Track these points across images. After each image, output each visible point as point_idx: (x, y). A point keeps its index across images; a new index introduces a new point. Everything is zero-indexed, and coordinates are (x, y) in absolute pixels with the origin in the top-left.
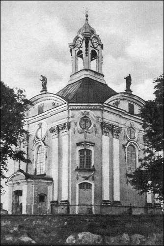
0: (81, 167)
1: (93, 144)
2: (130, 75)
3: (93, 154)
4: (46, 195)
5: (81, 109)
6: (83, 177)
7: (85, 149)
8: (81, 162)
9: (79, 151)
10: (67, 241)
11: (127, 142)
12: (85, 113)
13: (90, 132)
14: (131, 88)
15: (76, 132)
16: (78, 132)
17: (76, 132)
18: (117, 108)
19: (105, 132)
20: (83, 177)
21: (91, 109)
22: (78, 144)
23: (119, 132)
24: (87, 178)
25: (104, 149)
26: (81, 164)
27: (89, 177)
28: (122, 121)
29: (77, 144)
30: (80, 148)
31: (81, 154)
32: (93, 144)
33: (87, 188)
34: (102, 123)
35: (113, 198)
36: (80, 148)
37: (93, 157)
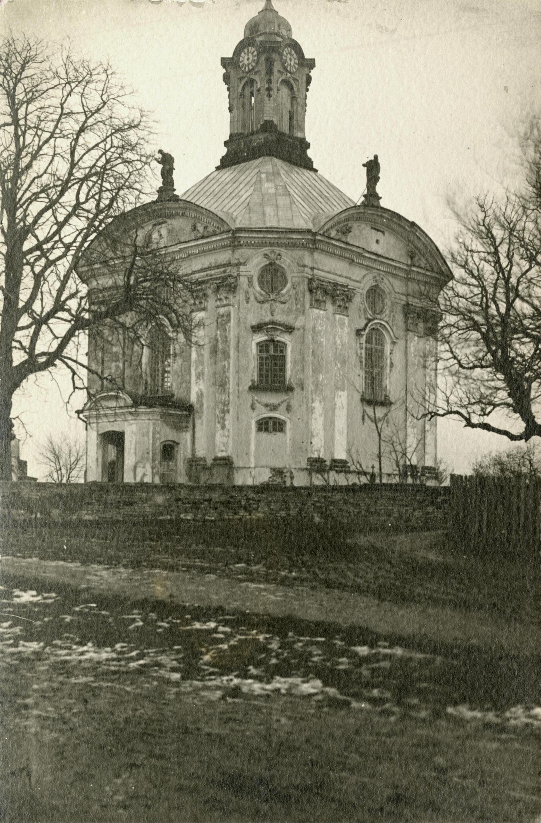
0: (261, 381)
1: (289, 329)
2: (376, 157)
3: (289, 349)
4: (178, 444)
5: (263, 245)
6: (266, 405)
7: (273, 341)
8: (260, 370)
9: (258, 344)
10: (15, 363)
11: (365, 322)
12: (272, 256)
13: (282, 299)
14: (379, 189)
15: (252, 298)
16: (256, 298)
17: (252, 298)
18: (347, 244)
19: (317, 301)
20: (266, 405)
21: (286, 246)
22: (257, 328)
23: (349, 299)
24: (274, 408)
25: (258, 226)
26: (260, 375)
27: (279, 405)
28: (357, 273)
29: (252, 327)
30: (261, 337)
31: (261, 351)
32: (289, 329)
33: (275, 430)
34: (311, 281)
35: (332, 453)
36: (261, 337)
37: (289, 359)
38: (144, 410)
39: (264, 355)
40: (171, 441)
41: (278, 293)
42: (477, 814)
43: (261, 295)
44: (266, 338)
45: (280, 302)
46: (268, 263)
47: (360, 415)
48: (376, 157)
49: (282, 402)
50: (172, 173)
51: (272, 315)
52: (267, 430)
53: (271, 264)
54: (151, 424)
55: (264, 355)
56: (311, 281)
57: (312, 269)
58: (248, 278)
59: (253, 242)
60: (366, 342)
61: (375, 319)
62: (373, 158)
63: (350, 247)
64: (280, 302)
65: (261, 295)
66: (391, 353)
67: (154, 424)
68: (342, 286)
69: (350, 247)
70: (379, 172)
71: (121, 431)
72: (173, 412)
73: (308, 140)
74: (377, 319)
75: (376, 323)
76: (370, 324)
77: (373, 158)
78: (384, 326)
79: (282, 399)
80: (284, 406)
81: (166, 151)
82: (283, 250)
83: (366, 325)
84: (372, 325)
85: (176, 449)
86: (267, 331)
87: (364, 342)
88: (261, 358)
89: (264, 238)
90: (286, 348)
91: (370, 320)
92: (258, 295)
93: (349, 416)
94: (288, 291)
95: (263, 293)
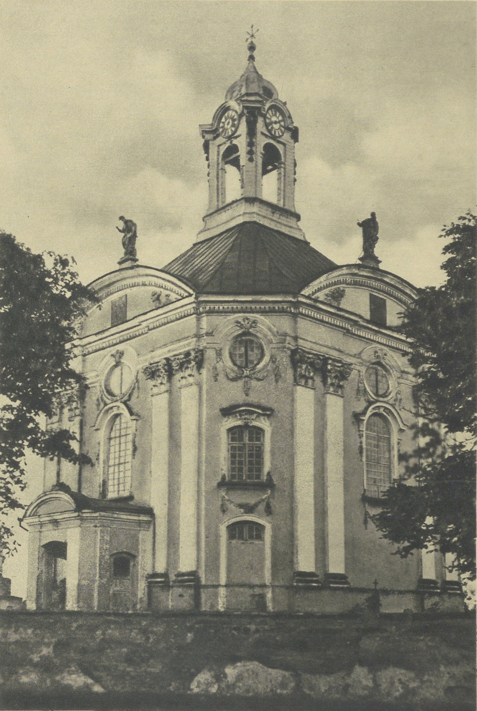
0: (233, 476)
2: (373, 215)
4: (134, 557)
6: (241, 506)
8: (233, 463)
13: (260, 376)
14: (378, 251)
20: (241, 506)
23: (343, 375)
30: (232, 422)
31: (233, 439)
33: (251, 537)
34: (294, 352)
36: (232, 422)
38: (88, 515)
39: (236, 444)
40: (126, 553)
41: (254, 368)
42: (377, 354)
43: (233, 371)
44: (239, 423)
45: (255, 378)
46: (240, 332)
47: (361, 518)
48: (373, 215)
49: (260, 502)
50: (135, 240)
51: (247, 395)
52: (241, 537)
53: (244, 334)
54: (99, 532)
55: (236, 444)
56: (294, 352)
57: (296, 338)
58: (217, 351)
59: (221, 308)
60: (367, 430)
61: (377, 401)
62: (369, 217)
63: (342, 313)
64: (255, 378)
65: (233, 371)
66: (399, 443)
67: (102, 531)
68: (334, 360)
69: (342, 313)
70: (377, 232)
71: (63, 541)
72: (125, 517)
73: (308, 241)
74: (380, 401)
75: (379, 407)
76: (370, 409)
77: (369, 217)
78: (390, 411)
79: (258, 499)
80: (261, 507)
81: (127, 218)
82: (258, 316)
83: (366, 409)
84: (373, 409)
85: (132, 564)
86: (241, 415)
87: (364, 429)
88: (233, 448)
89: (234, 302)
90: (264, 435)
91: (370, 403)
92: (228, 371)
93: (348, 520)
94: (265, 366)
95: (236, 368)
